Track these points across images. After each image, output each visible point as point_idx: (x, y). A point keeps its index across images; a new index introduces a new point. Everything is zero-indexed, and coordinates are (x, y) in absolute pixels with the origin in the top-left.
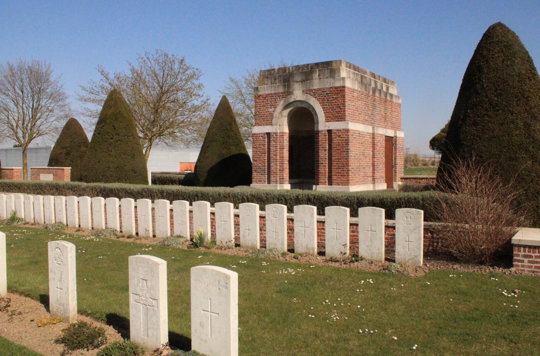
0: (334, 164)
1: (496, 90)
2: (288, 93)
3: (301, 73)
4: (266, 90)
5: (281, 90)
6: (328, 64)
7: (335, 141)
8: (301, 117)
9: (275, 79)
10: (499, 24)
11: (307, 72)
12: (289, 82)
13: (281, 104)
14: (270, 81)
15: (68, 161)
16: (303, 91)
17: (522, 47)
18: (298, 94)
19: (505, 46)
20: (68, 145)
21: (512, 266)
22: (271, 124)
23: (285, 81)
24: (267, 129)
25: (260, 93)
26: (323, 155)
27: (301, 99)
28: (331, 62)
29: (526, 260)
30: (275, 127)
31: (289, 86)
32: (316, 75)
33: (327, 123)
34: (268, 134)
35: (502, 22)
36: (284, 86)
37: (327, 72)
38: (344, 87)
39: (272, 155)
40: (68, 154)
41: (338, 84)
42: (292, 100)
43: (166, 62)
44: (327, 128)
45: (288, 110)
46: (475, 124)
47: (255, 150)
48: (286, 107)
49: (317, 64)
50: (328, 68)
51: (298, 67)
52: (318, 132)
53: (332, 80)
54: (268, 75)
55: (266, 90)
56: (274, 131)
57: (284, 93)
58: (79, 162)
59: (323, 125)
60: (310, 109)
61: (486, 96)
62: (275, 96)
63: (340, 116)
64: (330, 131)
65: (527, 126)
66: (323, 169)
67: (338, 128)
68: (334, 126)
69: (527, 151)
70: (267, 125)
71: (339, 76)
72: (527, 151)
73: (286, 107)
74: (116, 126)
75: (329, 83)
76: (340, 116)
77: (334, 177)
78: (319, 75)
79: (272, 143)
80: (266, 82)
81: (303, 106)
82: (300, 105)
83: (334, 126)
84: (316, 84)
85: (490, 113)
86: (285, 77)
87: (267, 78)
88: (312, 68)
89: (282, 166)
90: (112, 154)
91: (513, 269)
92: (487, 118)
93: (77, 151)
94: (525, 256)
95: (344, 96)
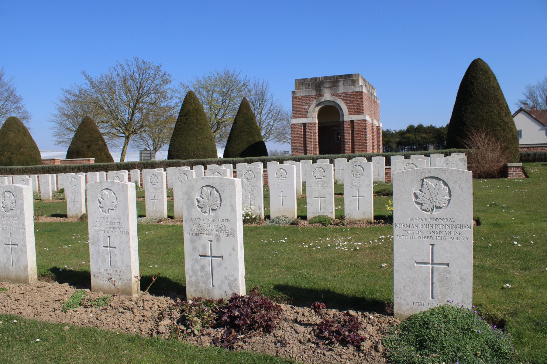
0: (356, 143)
1: (482, 95)
2: (320, 95)
3: (330, 82)
4: (302, 93)
5: (314, 93)
6: (349, 76)
7: (356, 127)
8: (329, 113)
9: (309, 86)
10: (479, 59)
11: (334, 81)
12: (320, 87)
13: (314, 103)
14: (304, 87)
15: (91, 154)
16: (331, 94)
17: (492, 72)
18: (327, 96)
19: (485, 72)
20: (88, 139)
21: (508, 176)
22: (307, 117)
23: (317, 87)
24: (304, 120)
25: (296, 95)
26: (348, 137)
27: (330, 100)
28: (352, 75)
29: (514, 173)
30: (309, 119)
31: (320, 91)
32: (341, 84)
33: (350, 116)
34: (304, 125)
35: (481, 58)
36: (316, 90)
37: (349, 82)
38: (362, 92)
39: (307, 139)
40: (89, 147)
41: (357, 90)
42: (323, 100)
43: (143, 69)
44: (350, 119)
45: (319, 107)
46: (472, 113)
47: (293, 135)
48: (318, 105)
49: (341, 76)
50: (350, 79)
51: (326, 78)
52: (343, 122)
53: (353, 87)
54: (302, 83)
55: (302, 93)
56: (309, 122)
57: (316, 95)
58: (99, 154)
59: (347, 117)
60: (337, 106)
61: (477, 98)
62: (310, 97)
63: (360, 111)
64: (352, 122)
65: (499, 113)
66: (348, 147)
67: (359, 119)
68: (355, 117)
69: (501, 126)
70: (303, 117)
71: (359, 84)
72: (501, 126)
73: (318, 105)
74: (198, 118)
75: (351, 89)
76: (360, 111)
77: (62, 213)
78: (343, 84)
79: (308, 130)
80: (301, 87)
81: (331, 104)
82: (328, 104)
83: (355, 117)
84: (342, 89)
85: (481, 107)
86: (318, 85)
87: (303, 84)
88: (337, 78)
89: (315, 146)
90: (198, 138)
91: (509, 178)
92: (479, 110)
93: (96, 144)
94: (514, 171)
95: (362, 98)
